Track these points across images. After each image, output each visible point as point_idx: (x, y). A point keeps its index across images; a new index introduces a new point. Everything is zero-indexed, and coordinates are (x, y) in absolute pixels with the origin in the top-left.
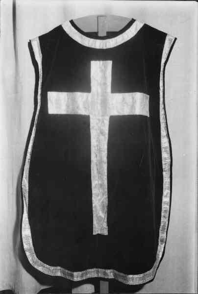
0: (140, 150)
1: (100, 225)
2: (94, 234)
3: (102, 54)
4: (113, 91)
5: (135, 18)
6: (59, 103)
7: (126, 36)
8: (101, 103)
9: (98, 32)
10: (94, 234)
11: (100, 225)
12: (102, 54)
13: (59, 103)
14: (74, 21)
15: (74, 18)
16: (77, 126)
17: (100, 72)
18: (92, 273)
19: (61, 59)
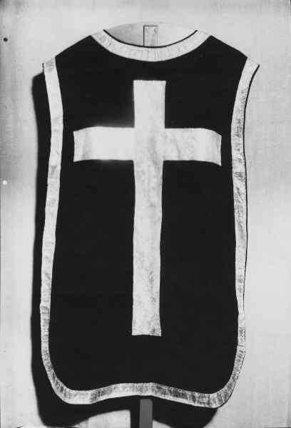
0: (201, 201)
1: (146, 318)
2: (135, 333)
3: (150, 71)
4: (169, 124)
5: (37, 72)
6: (199, 145)
7: (150, 55)
8: (146, 141)
9: (43, 73)
10: (135, 333)
11: (146, 318)
12: (150, 71)
13: (199, 145)
14: (94, 37)
15: (107, 28)
16: (119, 177)
17: (149, 97)
18: (122, 390)
19: (95, 81)
